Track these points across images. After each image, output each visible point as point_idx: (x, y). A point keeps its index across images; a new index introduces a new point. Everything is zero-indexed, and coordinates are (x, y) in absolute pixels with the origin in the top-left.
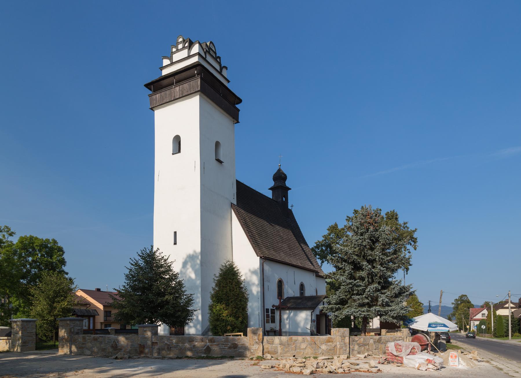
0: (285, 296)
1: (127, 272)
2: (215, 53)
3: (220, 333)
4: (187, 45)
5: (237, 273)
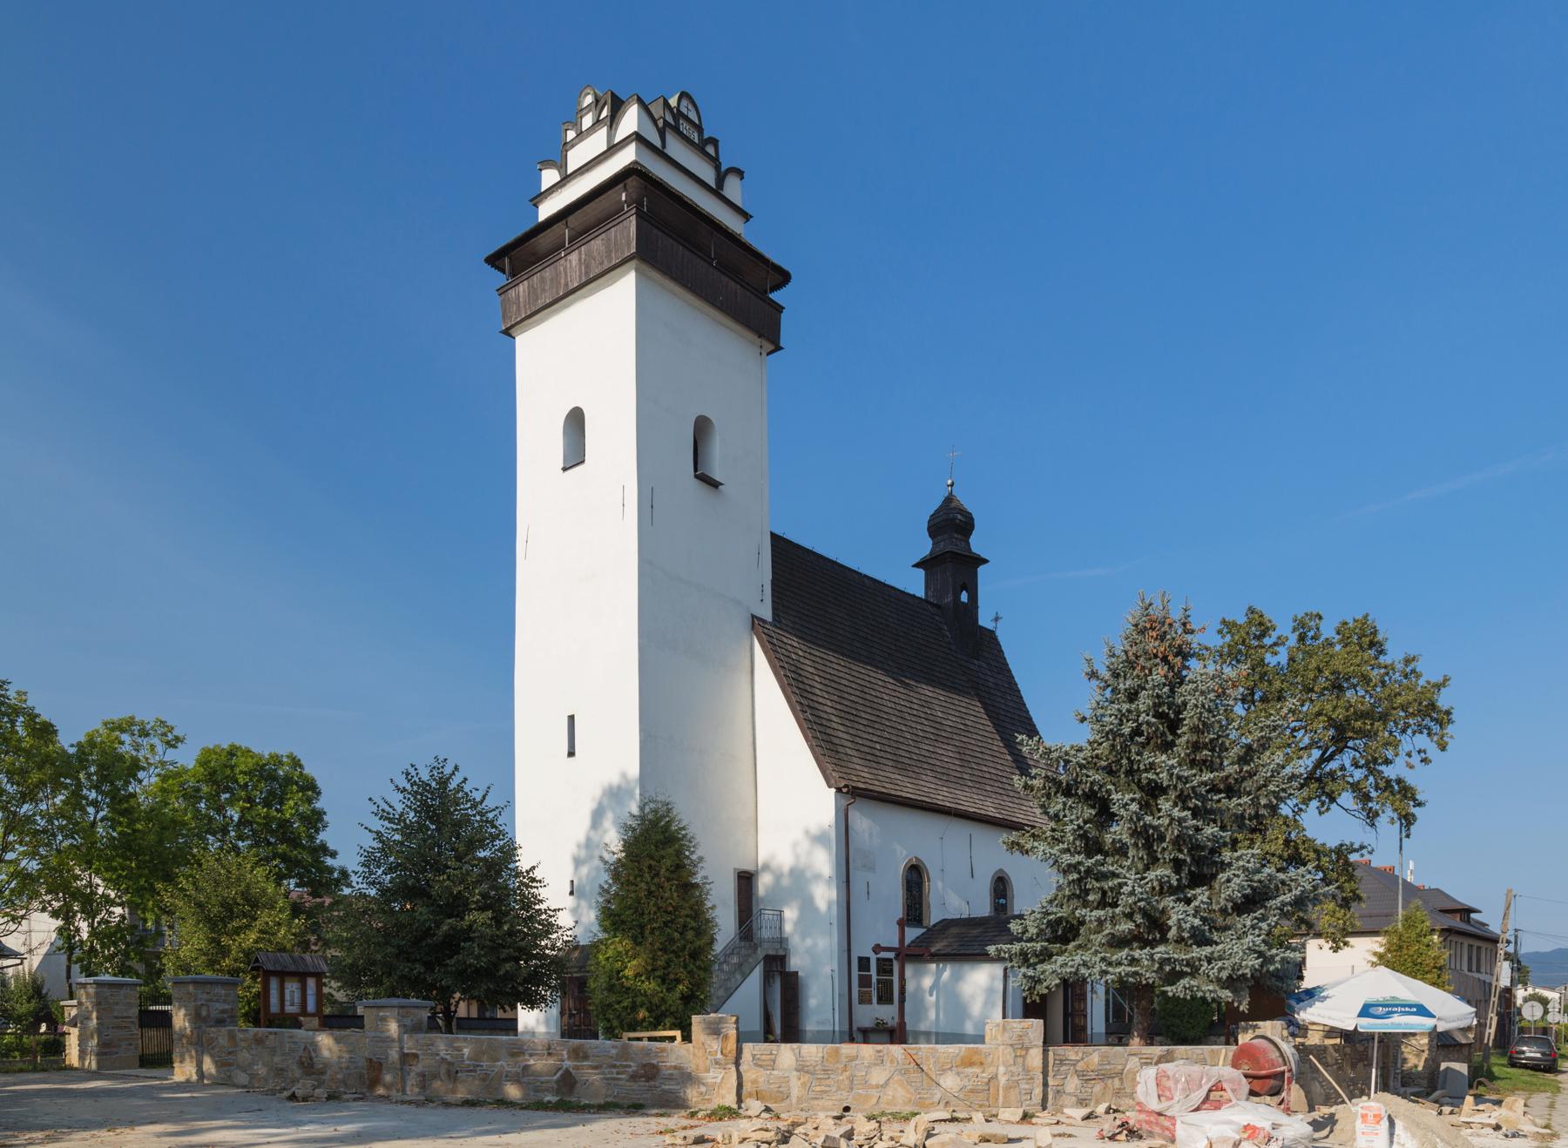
0: (935, 916)
2: (699, 128)
4: (605, 113)
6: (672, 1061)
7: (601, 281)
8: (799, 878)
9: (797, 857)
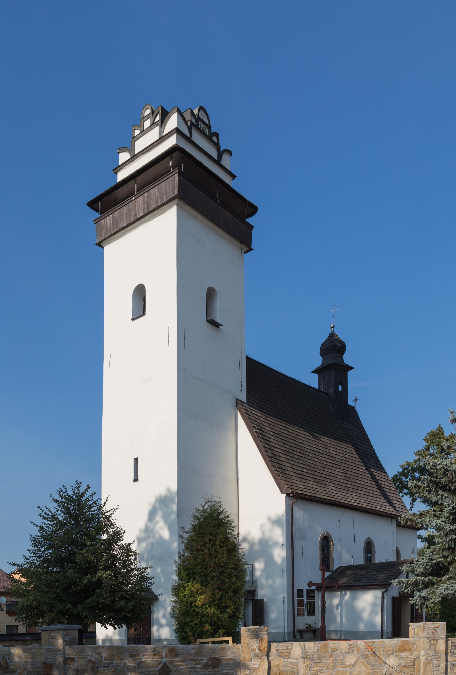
0: (336, 565)
1: (36, 532)
2: (209, 127)
3: (192, 639)
4: (158, 118)
5: (226, 523)
6: (229, 655)
7: (156, 212)
8: (265, 545)
9: (263, 533)
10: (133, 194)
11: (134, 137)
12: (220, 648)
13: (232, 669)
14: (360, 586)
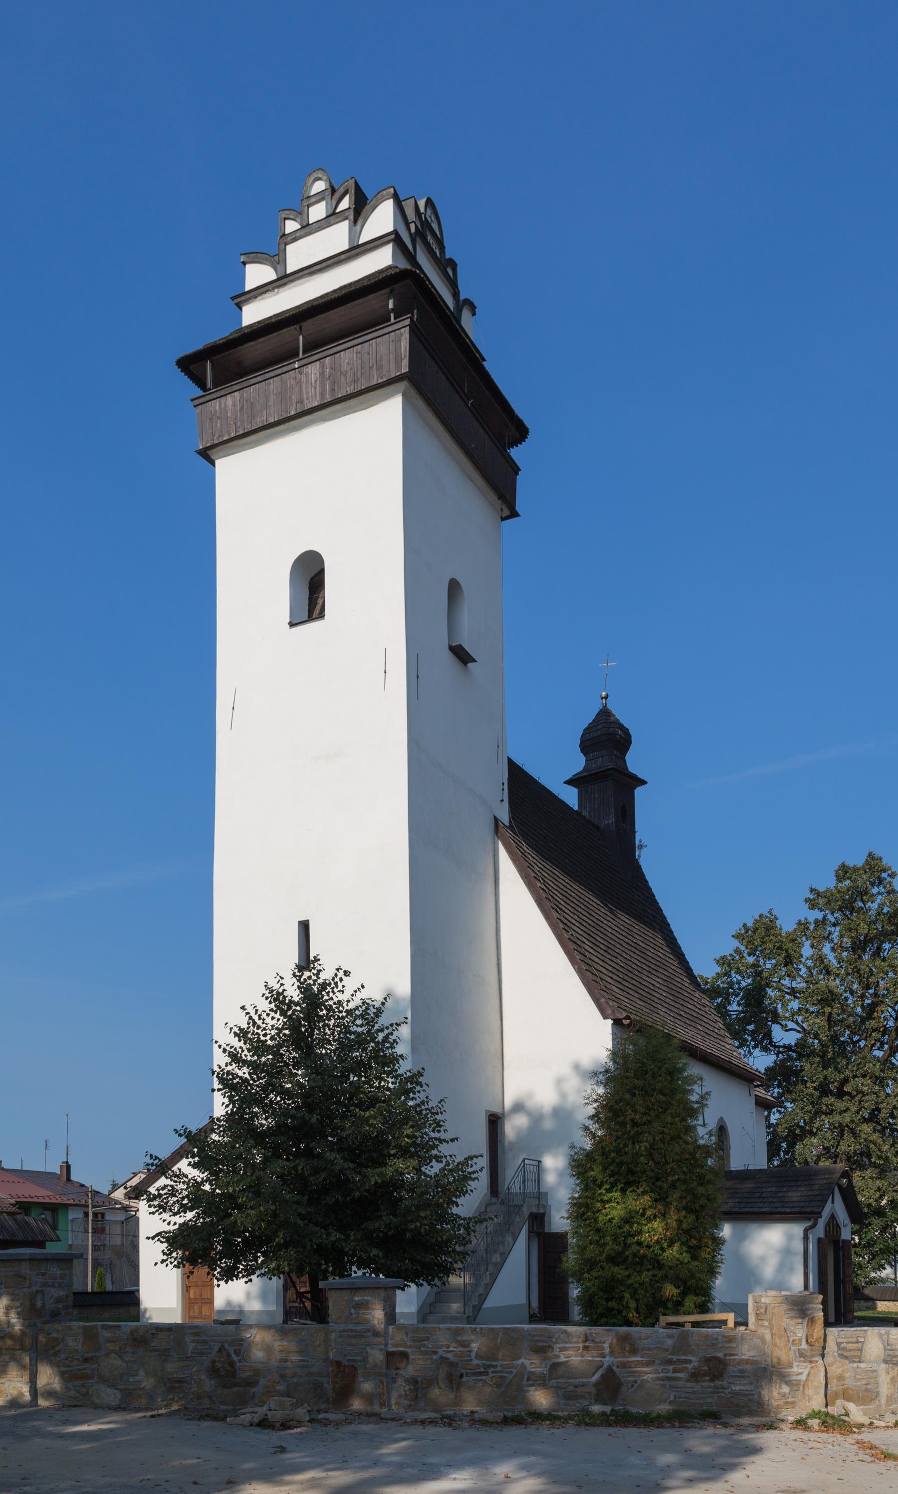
2: (442, 248)
4: (345, 204)
9: (563, 1095)
10: (293, 354)
11: (284, 235)
12: (726, 1337)
13: (751, 1383)
14: (744, 1213)
